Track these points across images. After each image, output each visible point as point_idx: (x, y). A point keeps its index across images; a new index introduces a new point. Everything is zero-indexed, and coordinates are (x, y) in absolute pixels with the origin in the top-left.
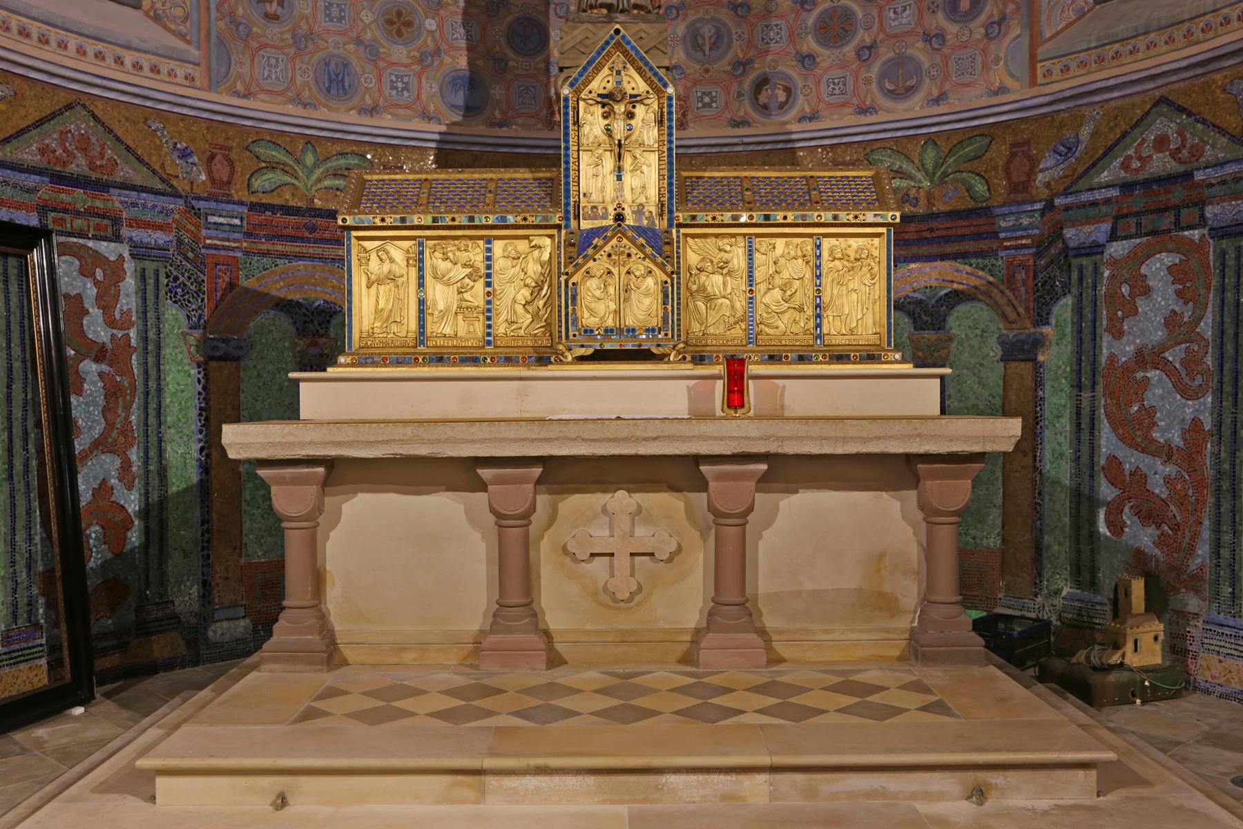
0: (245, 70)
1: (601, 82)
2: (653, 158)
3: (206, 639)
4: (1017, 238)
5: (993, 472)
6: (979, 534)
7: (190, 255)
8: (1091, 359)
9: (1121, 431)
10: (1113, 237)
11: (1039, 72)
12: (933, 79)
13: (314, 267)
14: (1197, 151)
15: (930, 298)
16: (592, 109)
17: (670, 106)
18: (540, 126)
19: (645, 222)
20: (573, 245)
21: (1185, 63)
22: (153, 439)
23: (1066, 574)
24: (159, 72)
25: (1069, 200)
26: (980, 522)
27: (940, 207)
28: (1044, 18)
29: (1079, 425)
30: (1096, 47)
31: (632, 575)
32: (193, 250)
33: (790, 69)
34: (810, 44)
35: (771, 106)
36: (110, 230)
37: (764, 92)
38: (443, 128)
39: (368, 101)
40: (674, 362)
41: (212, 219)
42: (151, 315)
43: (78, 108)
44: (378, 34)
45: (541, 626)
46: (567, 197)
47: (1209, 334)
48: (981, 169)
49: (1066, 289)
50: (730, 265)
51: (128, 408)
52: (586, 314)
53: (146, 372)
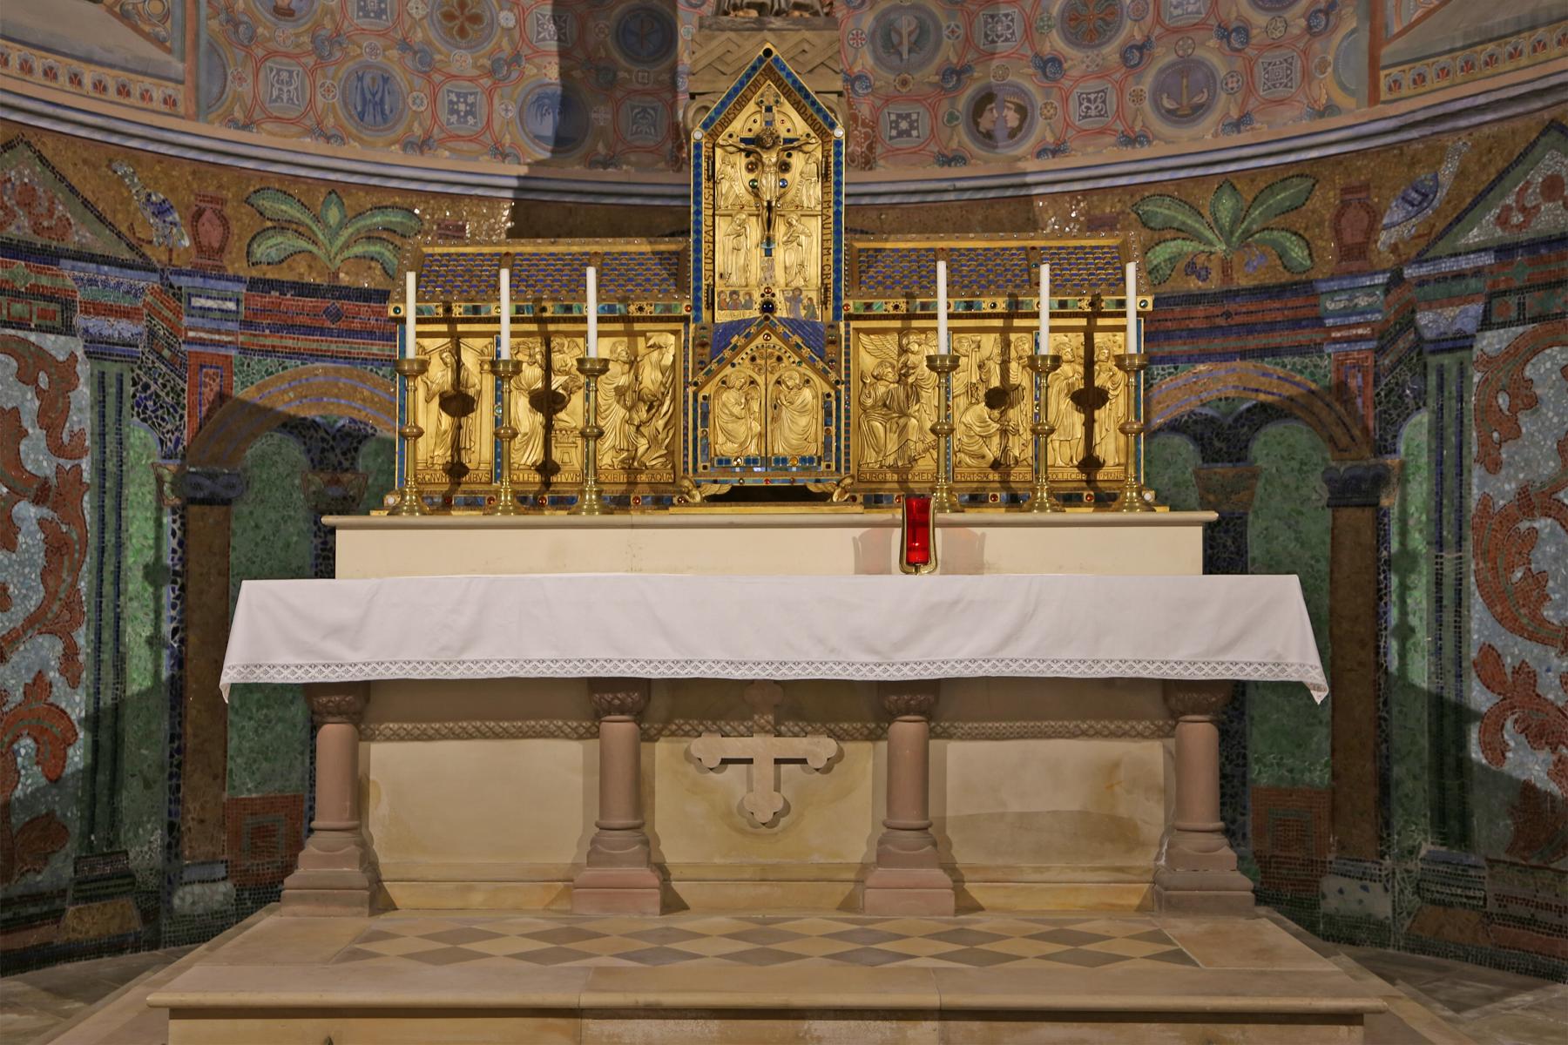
0: (246, 89)
1: (745, 122)
2: (815, 225)
3: (171, 910)
4: (1350, 327)
7: (166, 353)
8: (1456, 502)
9: (1499, 609)
10: (1486, 324)
11: (1383, 85)
13: (337, 371)
15: (1225, 415)
16: (732, 158)
17: (838, 154)
18: (662, 165)
19: (803, 313)
20: (703, 345)
22: (108, 616)
23: (1425, 823)
24: (128, 94)
25: (1424, 270)
26: (1299, 746)
27: (1242, 281)
29: (1439, 600)
30: (1463, 48)
31: (777, 789)
32: (170, 346)
34: (1055, 43)
36: (58, 318)
37: (987, 114)
38: (523, 170)
40: (838, 504)
41: (198, 302)
42: (111, 438)
43: (21, 147)
44: (432, 34)
45: (654, 859)
46: (698, 279)
48: (1300, 226)
49: (1420, 400)
50: (918, 371)
51: (75, 571)
52: (721, 439)
53: (102, 519)
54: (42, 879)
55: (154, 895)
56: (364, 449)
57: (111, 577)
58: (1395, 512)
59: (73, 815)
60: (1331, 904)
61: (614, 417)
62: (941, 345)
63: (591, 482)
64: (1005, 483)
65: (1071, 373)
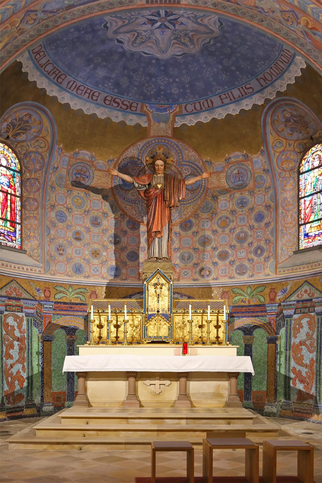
0: (54, 268)
1: (154, 281)
2: (167, 298)
3: (42, 410)
5: (265, 371)
6: (261, 387)
7: (39, 315)
10: (295, 313)
11: (278, 272)
12: (250, 271)
14: (313, 294)
21: (310, 274)
22: (30, 360)
23: (283, 396)
25: (285, 304)
27: (252, 304)
28: (279, 257)
33: (210, 265)
34: (216, 260)
35: (205, 275)
38: (108, 281)
39: (87, 274)
41: (45, 306)
44: (90, 257)
47: (315, 338)
52: (149, 333)
54: (20, 404)
55: (39, 408)
56: (77, 331)
57: (30, 354)
58: (279, 345)
59: (25, 394)
60: (266, 410)
61: (129, 329)
62: (190, 318)
63: (126, 339)
64: (202, 340)
65: (215, 323)
